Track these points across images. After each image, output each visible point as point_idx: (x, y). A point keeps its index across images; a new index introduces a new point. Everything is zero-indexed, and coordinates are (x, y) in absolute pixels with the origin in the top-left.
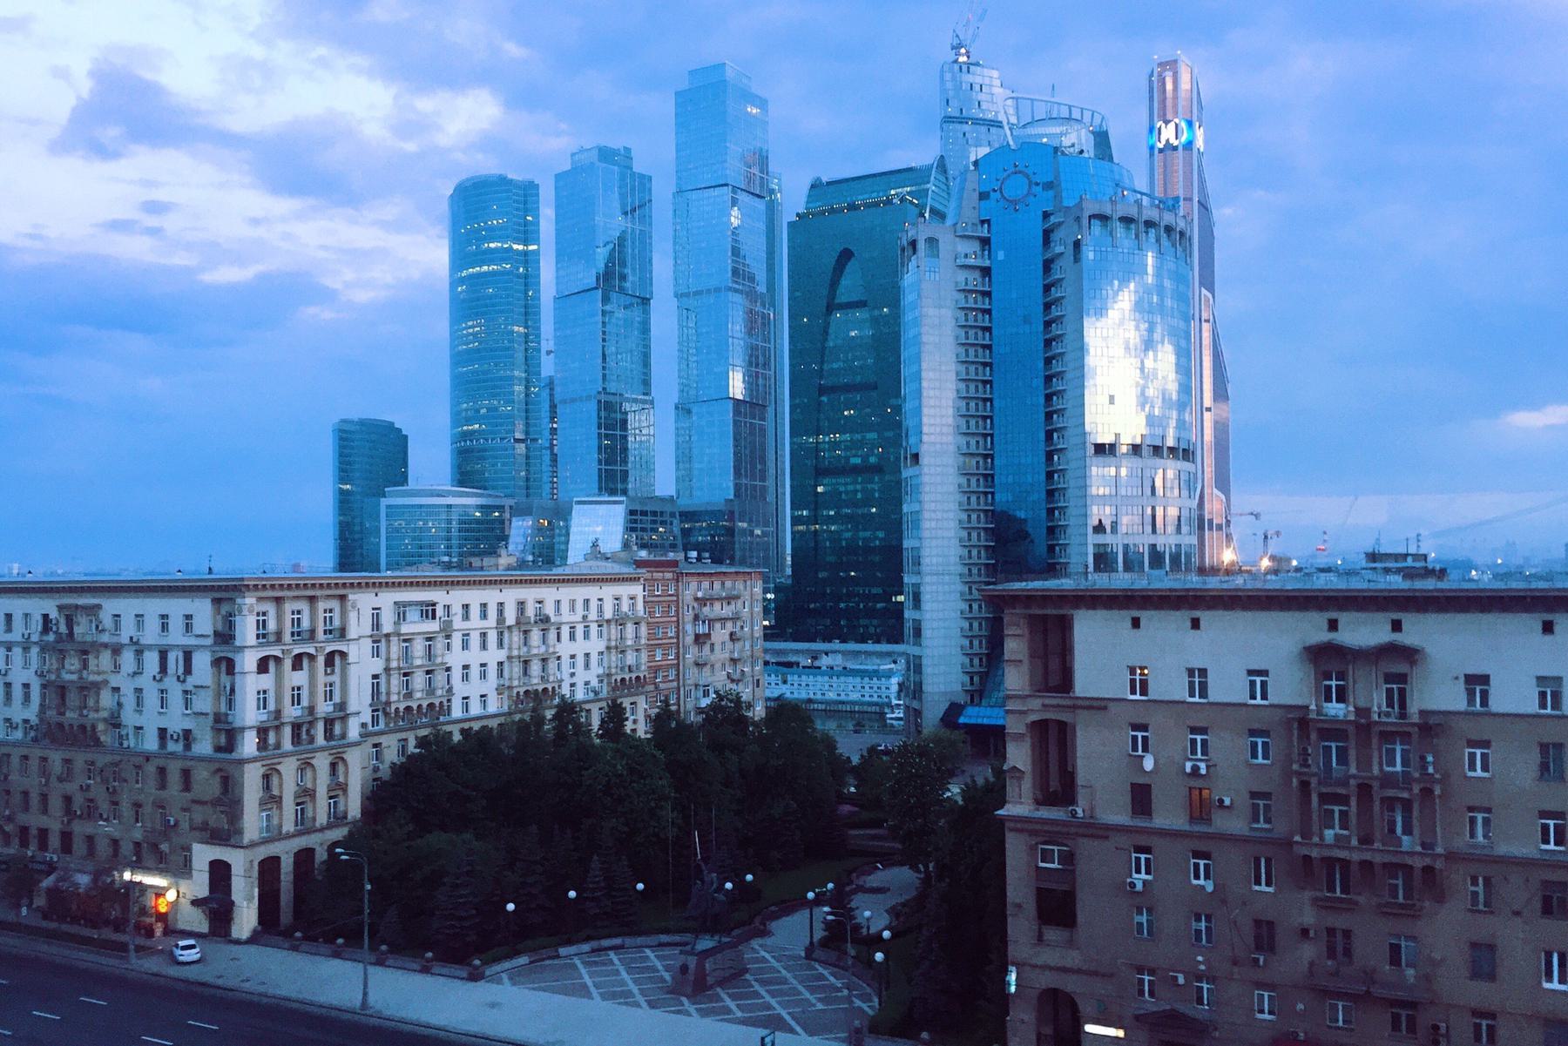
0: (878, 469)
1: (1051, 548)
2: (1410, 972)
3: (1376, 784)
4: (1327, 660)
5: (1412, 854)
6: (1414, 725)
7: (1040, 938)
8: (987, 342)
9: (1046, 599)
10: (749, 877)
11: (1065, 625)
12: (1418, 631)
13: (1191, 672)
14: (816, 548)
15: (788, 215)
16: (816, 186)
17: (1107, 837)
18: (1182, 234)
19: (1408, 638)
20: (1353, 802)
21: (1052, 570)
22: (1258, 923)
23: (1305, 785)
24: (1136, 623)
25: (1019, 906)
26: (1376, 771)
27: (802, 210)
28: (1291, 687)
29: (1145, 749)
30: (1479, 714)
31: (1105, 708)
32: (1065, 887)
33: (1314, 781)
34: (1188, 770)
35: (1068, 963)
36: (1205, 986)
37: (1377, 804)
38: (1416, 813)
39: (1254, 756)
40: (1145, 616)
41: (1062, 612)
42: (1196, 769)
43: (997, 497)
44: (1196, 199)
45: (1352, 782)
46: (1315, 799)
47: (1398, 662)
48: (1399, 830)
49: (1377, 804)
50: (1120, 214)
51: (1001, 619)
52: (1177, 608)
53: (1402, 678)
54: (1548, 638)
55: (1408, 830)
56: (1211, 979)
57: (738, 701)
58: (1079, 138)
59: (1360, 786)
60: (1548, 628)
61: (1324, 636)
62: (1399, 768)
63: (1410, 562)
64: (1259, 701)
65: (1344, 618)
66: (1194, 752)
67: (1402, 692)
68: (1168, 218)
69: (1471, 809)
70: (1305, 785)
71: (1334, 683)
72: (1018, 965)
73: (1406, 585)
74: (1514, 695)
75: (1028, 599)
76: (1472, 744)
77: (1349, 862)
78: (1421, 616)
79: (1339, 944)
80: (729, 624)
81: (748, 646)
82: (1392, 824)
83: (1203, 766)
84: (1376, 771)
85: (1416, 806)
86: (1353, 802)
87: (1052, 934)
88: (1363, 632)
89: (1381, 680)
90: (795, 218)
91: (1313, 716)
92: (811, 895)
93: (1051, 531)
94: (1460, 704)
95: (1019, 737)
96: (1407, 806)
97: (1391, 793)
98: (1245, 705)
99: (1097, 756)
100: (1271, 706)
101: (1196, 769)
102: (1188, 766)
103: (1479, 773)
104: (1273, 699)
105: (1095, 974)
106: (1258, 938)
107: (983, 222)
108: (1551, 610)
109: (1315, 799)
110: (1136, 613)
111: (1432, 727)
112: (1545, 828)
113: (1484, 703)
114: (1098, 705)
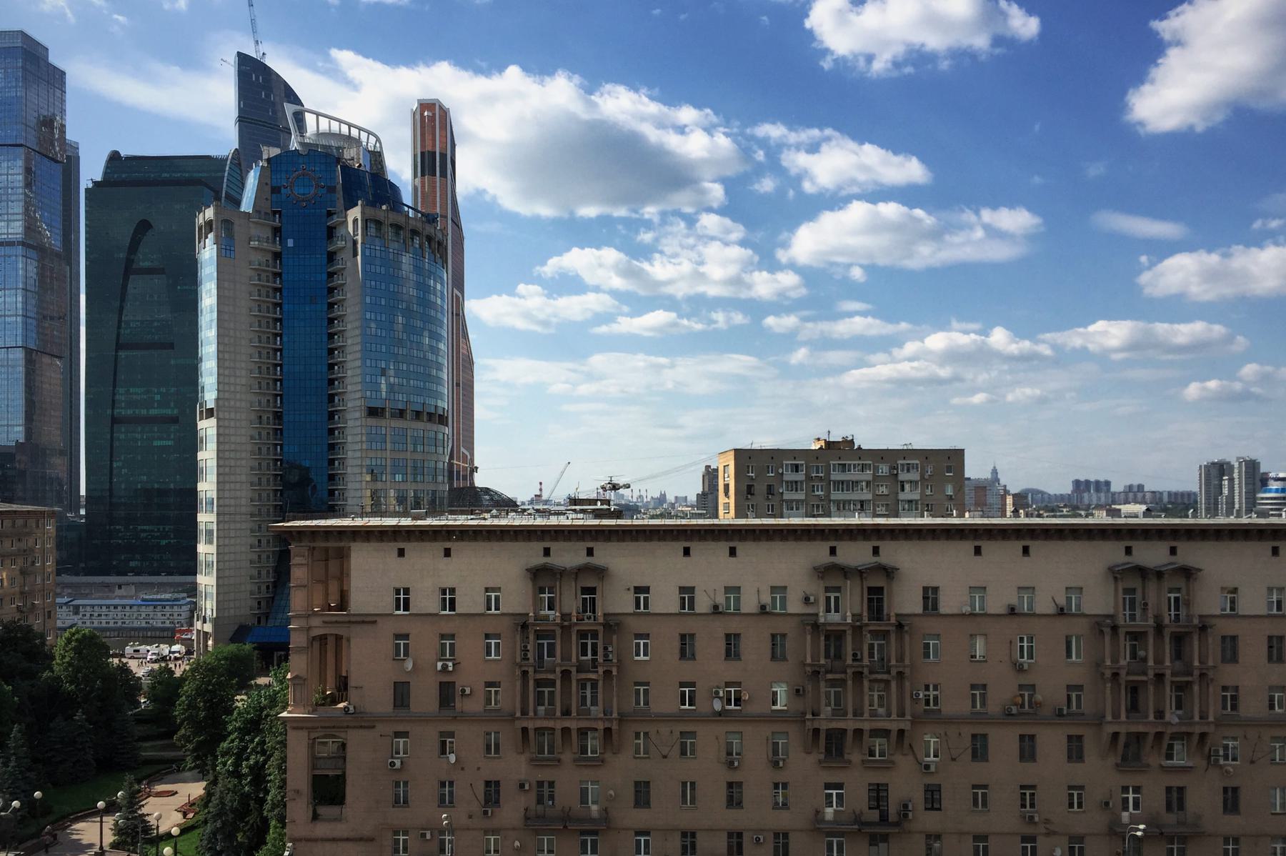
0: (174, 420)
1: (331, 493)
2: (594, 808)
3: (866, 671)
4: (541, 576)
5: (596, 719)
6: (892, 625)
7: (315, 817)
8: (278, 316)
9: (328, 533)
10: (37, 794)
11: (343, 555)
12: (607, 555)
13: (398, 592)
14: (111, 490)
15: (85, 183)
16: (114, 157)
17: (374, 727)
18: (440, 244)
19: (884, 559)
20: (558, 683)
21: (332, 511)
22: (488, 783)
23: (525, 673)
24: (733, 552)
25: (298, 792)
26: (574, 660)
27: (99, 178)
28: (516, 599)
29: (406, 654)
30: (642, 614)
31: (375, 622)
32: (339, 772)
33: (531, 670)
34: (439, 667)
35: (337, 834)
36: (402, 838)
37: (574, 684)
38: (600, 690)
39: (489, 654)
40: (407, 546)
41: (342, 544)
42: (445, 667)
43: (286, 448)
44: (449, 216)
45: (558, 669)
46: (531, 683)
47: (591, 579)
48: (589, 702)
49: (574, 684)
50: (391, 221)
51: (289, 552)
52: (435, 540)
53: (592, 591)
54: (687, 559)
55: (594, 703)
56: (452, 832)
57: (29, 629)
58: (358, 154)
59: (562, 672)
60: (1275, 551)
61: (543, 560)
62: (590, 656)
63: (599, 506)
64: (493, 611)
65: (554, 546)
66: (443, 653)
67: (646, 599)
68: (429, 229)
69: (637, 684)
70: (525, 673)
71: (546, 596)
72: (293, 840)
73: (596, 522)
74: (665, 600)
75: (314, 533)
76: (639, 636)
77: (553, 729)
78: (1060, 542)
79: (544, 791)
80: (20, 561)
81: (39, 580)
82: (584, 698)
83: (450, 664)
84: (574, 660)
85: (600, 683)
86: (558, 683)
87: (323, 810)
88: (568, 556)
89: (579, 592)
90: (90, 185)
91: (531, 620)
92: (101, 804)
93: (332, 478)
94: (631, 609)
95: (300, 650)
96: (594, 685)
97: (583, 676)
98: (391, 615)
99: (369, 665)
100: (503, 614)
101: (445, 667)
102: (439, 664)
103: (642, 657)
104: (503, 609)
105: (361, 839)
106: (487, 794)
107: (275, 213)
108: (689, 539)
109: (531, 683)
110: (590, 544)
111: (613, 625)
112: (683, 694)
113: (646, 607)
114: (368, 621)
